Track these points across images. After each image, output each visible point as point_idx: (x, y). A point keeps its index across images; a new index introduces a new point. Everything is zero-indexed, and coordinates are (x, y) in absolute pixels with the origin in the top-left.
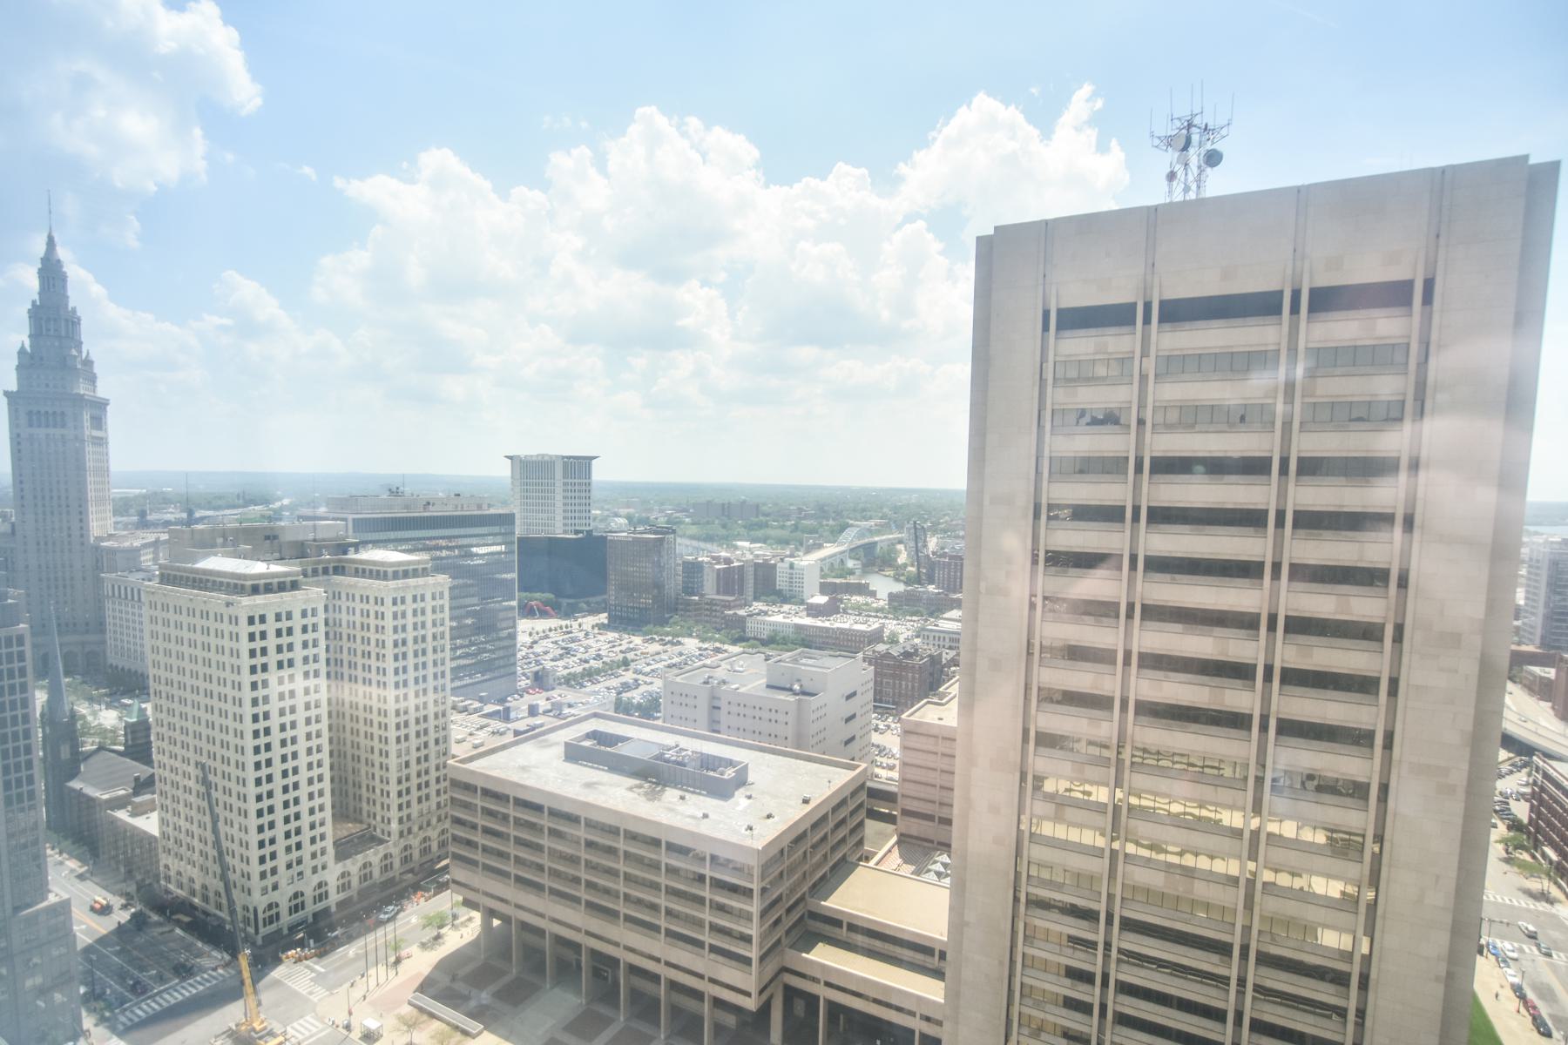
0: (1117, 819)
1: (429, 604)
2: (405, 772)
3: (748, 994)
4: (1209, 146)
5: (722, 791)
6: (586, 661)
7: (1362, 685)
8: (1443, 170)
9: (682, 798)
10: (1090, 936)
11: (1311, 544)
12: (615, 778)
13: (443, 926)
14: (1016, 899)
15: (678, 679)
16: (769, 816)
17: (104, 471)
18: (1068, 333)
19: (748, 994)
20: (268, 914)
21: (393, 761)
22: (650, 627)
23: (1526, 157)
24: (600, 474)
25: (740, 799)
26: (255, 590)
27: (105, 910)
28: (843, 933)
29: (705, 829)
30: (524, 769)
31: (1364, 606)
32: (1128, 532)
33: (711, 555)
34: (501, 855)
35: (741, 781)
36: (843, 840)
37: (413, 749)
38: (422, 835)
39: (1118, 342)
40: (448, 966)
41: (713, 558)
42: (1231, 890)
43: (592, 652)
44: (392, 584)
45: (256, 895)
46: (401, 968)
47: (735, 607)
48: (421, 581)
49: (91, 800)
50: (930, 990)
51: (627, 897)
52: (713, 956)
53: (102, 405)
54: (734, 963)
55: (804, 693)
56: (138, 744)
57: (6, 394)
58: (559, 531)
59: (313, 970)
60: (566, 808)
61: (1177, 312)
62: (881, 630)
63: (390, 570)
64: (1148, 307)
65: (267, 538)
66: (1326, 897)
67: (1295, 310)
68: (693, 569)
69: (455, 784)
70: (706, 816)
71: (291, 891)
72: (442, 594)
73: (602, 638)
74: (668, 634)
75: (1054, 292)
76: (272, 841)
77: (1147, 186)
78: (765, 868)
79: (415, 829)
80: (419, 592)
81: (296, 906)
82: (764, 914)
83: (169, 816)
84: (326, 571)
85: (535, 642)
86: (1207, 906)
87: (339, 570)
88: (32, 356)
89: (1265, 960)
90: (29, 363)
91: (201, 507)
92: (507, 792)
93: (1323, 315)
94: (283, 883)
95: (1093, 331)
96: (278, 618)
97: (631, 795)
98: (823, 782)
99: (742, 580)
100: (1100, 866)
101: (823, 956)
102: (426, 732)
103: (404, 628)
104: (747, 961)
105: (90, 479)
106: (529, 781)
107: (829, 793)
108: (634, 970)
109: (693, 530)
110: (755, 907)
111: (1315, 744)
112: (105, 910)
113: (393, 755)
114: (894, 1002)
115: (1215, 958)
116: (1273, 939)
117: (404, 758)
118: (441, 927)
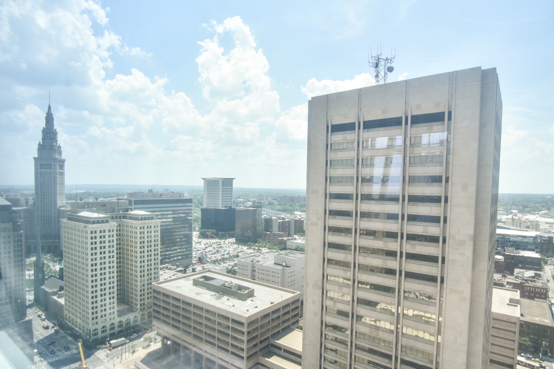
0: (398, 318)
1: (153, 229)
2: (143, 288)
4: (389, 65)
5: (243, 298)
6: (224, 255)
7: (433, 259)
8: (453, 73)
9: (228, 299)
12: (208, 291)
13: (150, 343)
14: (321, 336)
15: (242, 260)
16: (256, 307)
17: (63, 184)
20: (94, 332)
21: (139, 284)
22: (250, 243)
23: (480, 67)
25: (249, 301)
26: (94, 223)
27: (47, 328)
29: (232, 310)
30: (178, 287)
31: (433, 230)
33: (277, 216)
34: (168, 316)
35: (251, 294)
36: (288, 320)
37: (146, 280)
38: (148, 311)
40: (150, 355)
41: (278, 217)
42: (391, 335)
43: (227, 252)
44: (140, 222)
45: (91, 325)
46: (134, 354)
47: (283, 237)
48: (150, 221)
49: (47, 292)
51: (206, 333)
52: (232, 355)
53: (63, 161)
55: (287, 267)
56: (61, 275)
57: (34, 158)
58: (221, 207)
59: (106, 352)
60: (188, 301)
63: (140, 217)
64: (407, 118)
65: (102, 206)
67: (406, 123)
68: (268, 223)
69: (155, 291)
70: (234, 306)
71: (102, 325)
72: (157, 226)
73: (231, 247)
74: (256, 246)
75: (362, 115)
76: (96, 307)
77: (365, 80)
78: (250, 324)
79: (146, 308)
80: (149, 225)
81: (104, 331)
82: (248, 341)
83: (67, 298)
84: (120, 217)
85: (206, 248)
86: (384, 341)
87: (125, 217)
88: (42, 146)
90: (41, 148)
91: (101, 197)
92: (170, 294)
93: (416, 125)
94: (99, 322)
95: (342, 132)
96: (101, 232)
97: (211, 297)
99: (289, 227)
100: (392, 338)
102: (151, 274)
103: (144, 238)
104: (242, 358)
105: (58, 186)
106: (178, 291)
107: (281, 301)
108: (208, 359)
109: (279, 207)
110: (245, 338)
111: (418, 281)
112: (47, 328)
113: (139, 281)
115: (387, 361)
116: (406, 354)
117: (143, 283)
118: (151, 342)
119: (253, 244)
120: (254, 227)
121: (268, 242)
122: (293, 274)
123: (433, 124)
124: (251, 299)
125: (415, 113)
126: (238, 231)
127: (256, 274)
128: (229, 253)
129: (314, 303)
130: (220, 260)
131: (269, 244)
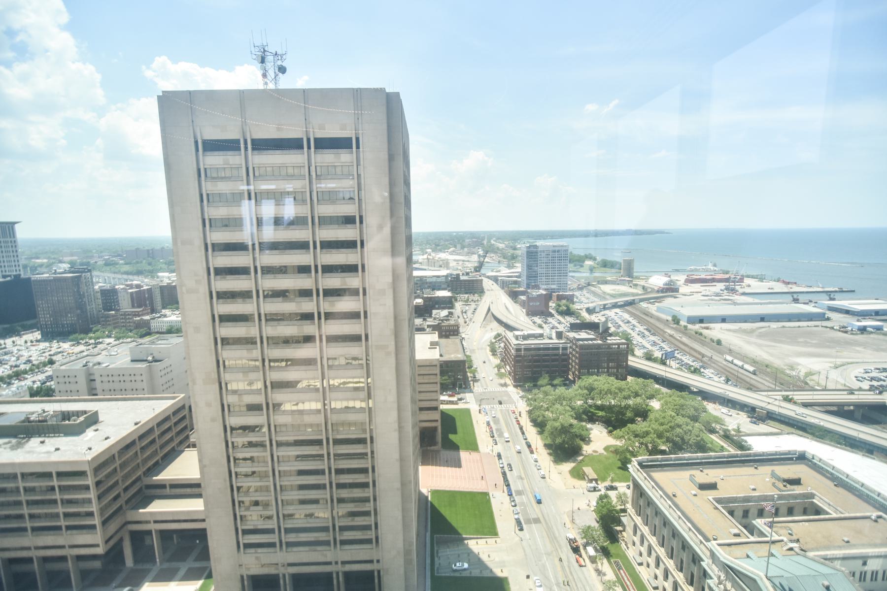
0: (324, 394)
3: (98, 546)
4: (279, 63)
9: (42, 442)
10: (320, 452)
11: (328, 256)
15: (63, 367)
16: (106, 439)
18: (209, 153)
19: (98, 546)
24: (22, 233)
25: (90, 433)
28: (168, 491)
29: (55, 457)
32: (251, 255)
33: (125, 283)
39: (235, 159)
41: (127, 285)
43: (23, 360)
47: (143, 315)
50: (195, 505)
52: (69, 532)
54: (84, 531)
61: (261, 145)
62: (824, 314)
66: (310, 410)
68: (109, 297)
70: (57, 449)
74: (90, 338)
78: (97, 470)
82: (99, 497)
86: (311, 426)
89: (337, 442)
95: (221, 153)
98: (145, 411)
101: (159, 507)
104: (93, 527)
109: (127, 268)
110: (92, 495)
114: (176, 518)
115: (317, 447)
119: (82, 336)
120: (81, 306)
121: (115, 328)
122: (169, 370)
123: (340, 151)
124: (94, 427)
125: (320, 135)
126: (44, 317)
127: (98, 385)
128: (29, 361)
129: (209, 405)
130: (10, 377)
131: (117, 330)
